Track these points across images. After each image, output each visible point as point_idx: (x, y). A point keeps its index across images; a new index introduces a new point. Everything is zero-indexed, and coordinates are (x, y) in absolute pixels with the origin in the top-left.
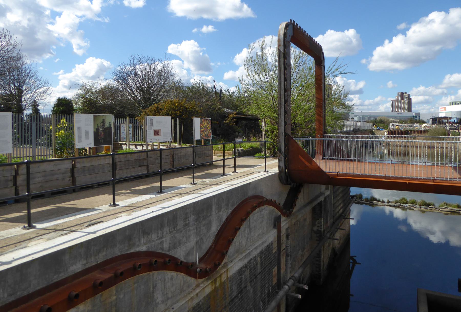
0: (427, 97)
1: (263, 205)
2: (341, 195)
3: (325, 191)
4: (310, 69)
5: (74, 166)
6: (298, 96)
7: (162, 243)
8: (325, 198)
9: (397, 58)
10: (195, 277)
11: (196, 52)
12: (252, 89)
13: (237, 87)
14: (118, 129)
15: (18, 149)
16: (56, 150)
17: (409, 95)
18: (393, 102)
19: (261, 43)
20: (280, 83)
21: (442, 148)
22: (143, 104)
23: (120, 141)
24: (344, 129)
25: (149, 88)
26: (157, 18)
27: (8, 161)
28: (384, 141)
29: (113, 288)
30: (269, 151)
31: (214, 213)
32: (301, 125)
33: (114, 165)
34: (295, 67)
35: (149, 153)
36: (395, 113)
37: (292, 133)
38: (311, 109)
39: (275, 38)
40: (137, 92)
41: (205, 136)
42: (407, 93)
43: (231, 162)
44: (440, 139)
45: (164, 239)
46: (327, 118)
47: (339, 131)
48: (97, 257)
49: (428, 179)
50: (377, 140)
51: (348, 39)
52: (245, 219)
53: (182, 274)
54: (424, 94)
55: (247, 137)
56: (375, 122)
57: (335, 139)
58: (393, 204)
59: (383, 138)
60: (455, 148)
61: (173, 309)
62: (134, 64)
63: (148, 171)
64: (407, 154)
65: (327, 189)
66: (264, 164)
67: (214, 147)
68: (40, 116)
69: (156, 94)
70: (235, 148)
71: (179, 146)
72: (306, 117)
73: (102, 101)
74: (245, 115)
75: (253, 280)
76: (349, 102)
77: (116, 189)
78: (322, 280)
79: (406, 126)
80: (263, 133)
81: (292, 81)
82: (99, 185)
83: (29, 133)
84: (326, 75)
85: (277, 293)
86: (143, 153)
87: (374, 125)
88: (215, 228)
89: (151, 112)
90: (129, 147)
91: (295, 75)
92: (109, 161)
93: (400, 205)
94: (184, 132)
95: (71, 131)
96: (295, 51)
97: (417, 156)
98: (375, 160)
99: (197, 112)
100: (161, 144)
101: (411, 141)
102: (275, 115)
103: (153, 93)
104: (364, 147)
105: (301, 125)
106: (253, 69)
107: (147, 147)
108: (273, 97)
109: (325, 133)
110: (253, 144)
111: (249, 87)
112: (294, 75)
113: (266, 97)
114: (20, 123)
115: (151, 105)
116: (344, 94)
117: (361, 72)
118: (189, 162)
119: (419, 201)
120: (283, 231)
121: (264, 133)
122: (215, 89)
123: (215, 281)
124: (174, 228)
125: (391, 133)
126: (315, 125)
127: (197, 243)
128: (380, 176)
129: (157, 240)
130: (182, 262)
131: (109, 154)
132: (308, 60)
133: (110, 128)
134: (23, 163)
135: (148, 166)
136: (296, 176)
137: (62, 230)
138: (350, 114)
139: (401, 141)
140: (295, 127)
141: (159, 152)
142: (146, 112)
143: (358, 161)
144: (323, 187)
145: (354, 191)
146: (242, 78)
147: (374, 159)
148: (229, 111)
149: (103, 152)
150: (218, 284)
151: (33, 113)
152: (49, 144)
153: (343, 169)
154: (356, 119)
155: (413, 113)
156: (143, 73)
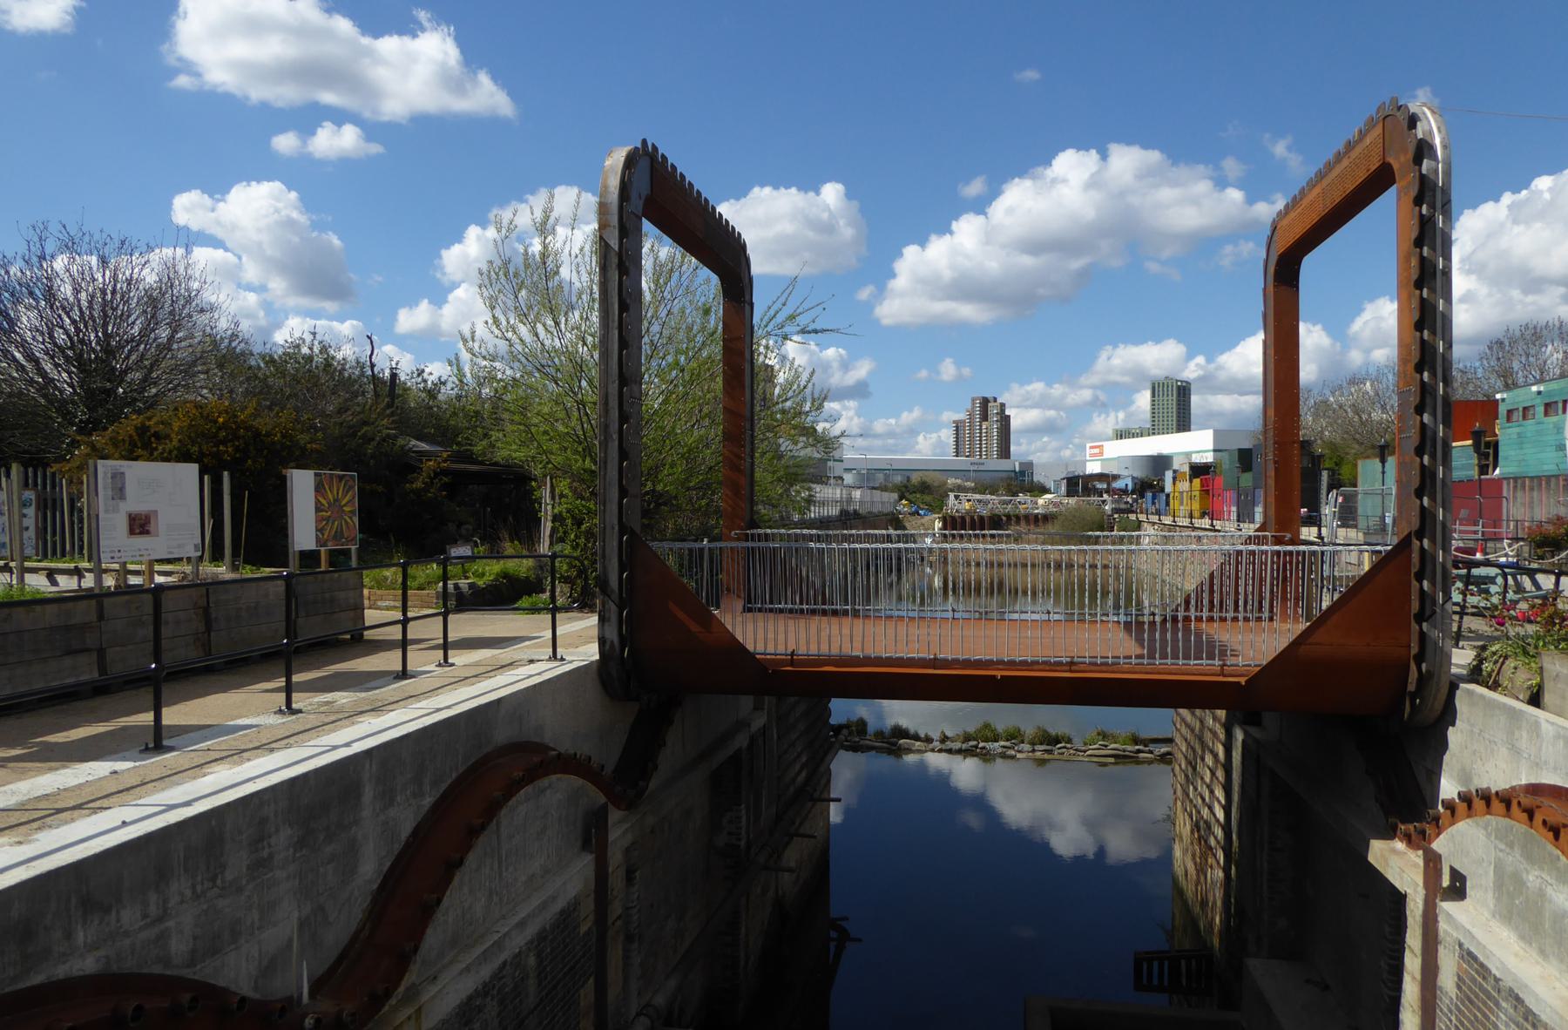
0: (1052, 413)
1: (547, 775)
4: (707, 312)
8: (752, 739)
9: (965, 288)
11: (290, 224)
12: (505, 371)
13: (455, 362)
17: (1003, 406)
18: (958, 427)
19: (538, 214)
20: (605, 355)
21: (1093, 566)
22: (81, 414)
24: (814, 513)
28: (930, 550)
31: (366, 813)
34: (659, 300)
35: (107, 601)
36: (963, 462)
37: (644, 527)
38: (707, 446)
39: (590, 200)
41: (335, 537)
42: (1000, 400)
46: (757, 475)
47: (796, 517)
51: (825, 216)
52: (483, 827)
57: (784, 544)
58: (957, 745)
59: (928, 540)
60: (1129, 568)
64: (999, 589)
66: (549, 634)
67: (368, 577)
70: (445, 578)
71: (230, 576)
72: (690, 472)
74: (482, 463)
76: (827, 425)
79: (994, 503)
81: (646, 349)
84: (758, 332)
86: (83, 604)
88: (370, 867)
89: (115, 445)
90: (21, 579)
91: (655, 328)
94: (252, 523)
96: (657, 249)
97: (1025, 593)
98: (908, 609)
99: (303, 449)
100: (157, 568)
104: (872, 569)
106: (510, 303)
107: (99, 580)
110: (511, 565)
111: (497, 365)
112: (653, 330)
113: (557, 403)
115: (114, 417)
116: (814, 400)
117: (858, 330)
118: (272, 631)
119: (1029, 731)
120: (615, 858)
121: (549, 524)
122: (373, 366)
124: (213, 879)
125: (951, 522)
126: (720, 499)
127: (302, 924)
130: (243, 1000)
132: (699, 280)
135: (101, 653)
136: (660, 671)
138: (830, 464)
139: (979, 548)
140: (657, 504)
141: (149, 597)
143: (856, 614)
144: (747, 702)
145: (842, 709)
146: (473, 333)
147: (904, 605)
148: (424, 446)
153: (808, 643)
154: (849, 478)
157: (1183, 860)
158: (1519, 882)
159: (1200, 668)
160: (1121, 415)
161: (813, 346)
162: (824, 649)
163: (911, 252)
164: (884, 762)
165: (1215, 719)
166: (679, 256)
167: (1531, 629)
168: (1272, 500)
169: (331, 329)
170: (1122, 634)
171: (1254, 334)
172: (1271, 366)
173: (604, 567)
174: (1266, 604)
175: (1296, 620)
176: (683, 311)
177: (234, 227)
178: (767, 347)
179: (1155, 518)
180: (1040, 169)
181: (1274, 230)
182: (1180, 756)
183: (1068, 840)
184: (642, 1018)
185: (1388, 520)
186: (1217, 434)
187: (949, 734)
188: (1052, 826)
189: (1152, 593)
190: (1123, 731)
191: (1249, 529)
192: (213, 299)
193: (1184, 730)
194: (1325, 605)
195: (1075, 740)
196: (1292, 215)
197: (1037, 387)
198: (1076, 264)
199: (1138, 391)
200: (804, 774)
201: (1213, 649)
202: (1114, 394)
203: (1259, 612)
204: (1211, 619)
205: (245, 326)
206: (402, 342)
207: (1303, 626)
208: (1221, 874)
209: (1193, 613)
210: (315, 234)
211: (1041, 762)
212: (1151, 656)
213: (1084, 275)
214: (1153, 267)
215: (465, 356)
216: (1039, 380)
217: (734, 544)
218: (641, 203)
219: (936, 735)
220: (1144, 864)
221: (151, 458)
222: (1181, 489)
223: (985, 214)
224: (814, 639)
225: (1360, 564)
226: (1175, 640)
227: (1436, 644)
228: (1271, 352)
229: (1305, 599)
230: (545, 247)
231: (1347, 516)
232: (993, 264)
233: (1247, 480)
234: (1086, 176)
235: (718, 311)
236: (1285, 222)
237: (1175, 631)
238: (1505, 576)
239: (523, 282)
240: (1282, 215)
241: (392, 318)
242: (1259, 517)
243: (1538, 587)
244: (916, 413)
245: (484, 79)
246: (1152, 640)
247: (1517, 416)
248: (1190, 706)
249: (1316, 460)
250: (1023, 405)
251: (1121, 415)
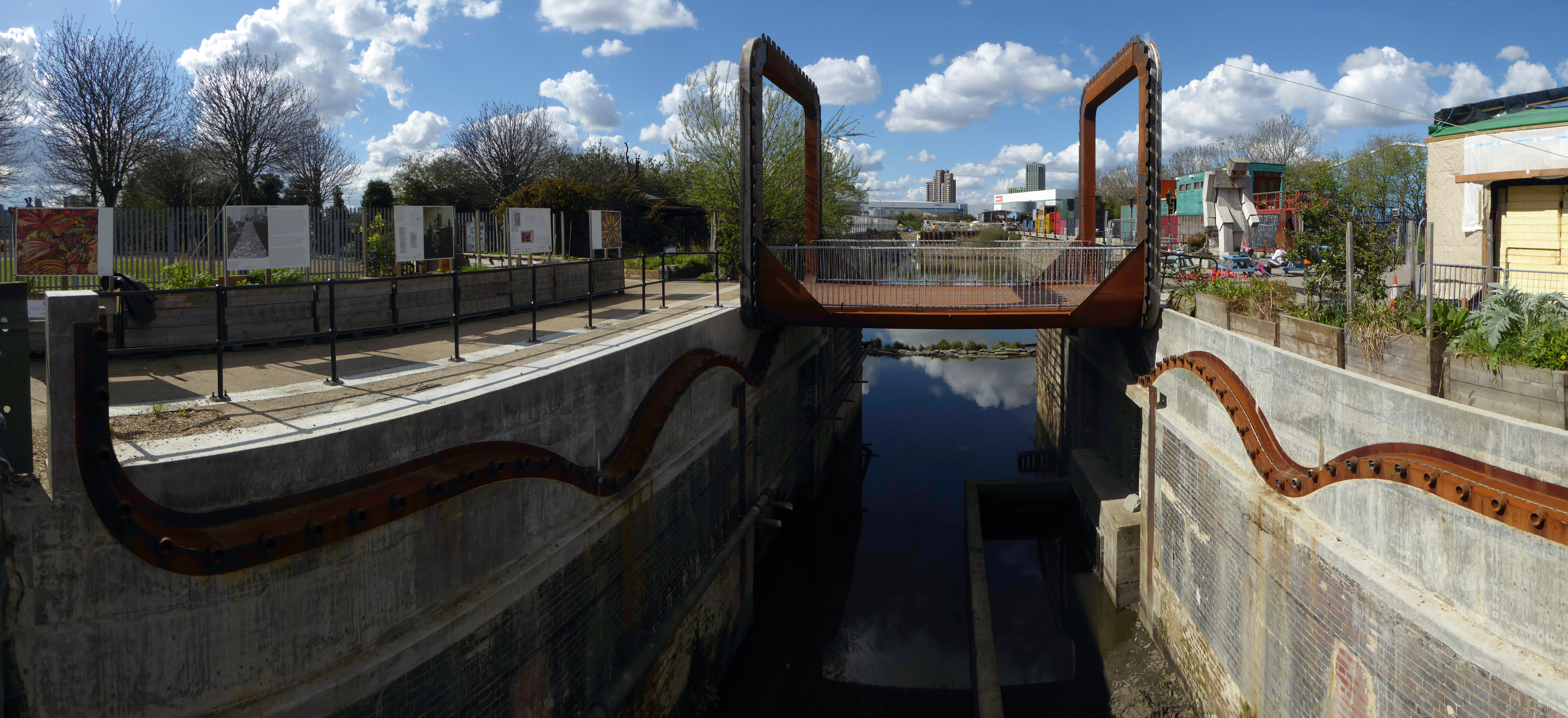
0: (977, 179)
1: (714, 366)
3: (820, 336)
4: (797, 125)
5: (394, 291)
6: (775, 172)
7: (537, 429)
8: (821, 350)
9: (933, 113)
10: (595, 493)
11: (590, 91)
12: (692, 158)
13: (667, 154)
14: (461, 230)
15: (317, 262)
16: (369, 264)
17: (952, 175)
18: (929, 186)
20: (743, 148)
21: (998, 258)
22: (502, 187)
23: (465, 251)
24: (853, 231)
25: (513, 158)
26: (524, 40)
27: (304, 280)
28: (914, 250)
29: (459, 498)
30: (724, 269)
31: (627, 380)
32: (781, 223)
33: (456, 292)
34: (771, 119)
35: (513, 272)
36: (931, 204)
37: (764, 238)
38: (797, 196)
39: (735, 67)
40: (492, 166)
43: (656, 289)
44: (995, 245)
45: (541, 423)
46: (824, 211)
47: (844, 233)
48: (432, 444)
51: (859, 73)
52: (683, 392)
53: (572, 486)
54: (971, 174)
55: (685, 245)
56: (901, 219)
58: (928, 352)
59: (913, 245)
60: (1015, 258)
61: (557, 546)
62: (486, 118)
63: (512, 304)
64: (949, 271)
66: (715, 293)
67: (626, 263)
68: (345, 211)
69: (524, 168)
70: (663, 264)
71: (564, 261)
72: (788, 210)
73: (436, 184)
74: (681, 205)
76: (860, 185)
77: (460, 332)
79: (947, 225)
80: (714, 238)
81: (765, 145)
82: (432, 325)
83: (331, 236)
84: (824, 135)
85: (740, 520)
86: (504, 273)
88: (629, 407)
89: (516, 201)
90: (480, 261)
91: (770, 134)
92: (449, 284)
94: (573, 237)
95: (390, 234)
96: (770, 92)
97: (963, 272)
98: (903, 281)
99: (596, 200)
100: (534, 257)
101: (955, 249)
102: (735, 205)
103: (519, 167)
104: (884, 260)
105: (781, 223)
107: (510, 262)
108: (731, 174)
109: (822, 237)
110: (695, 257)
111: (689, 155)
112: (768, 135)
113: (718, 174)
114: (318, 222)
115: (515, 188)
116: (853, 171)
117: (876, 134)
119: (965, 343)
120: (749, 411)
121: (715, 237)
122: (628, 158)
123: (630, 501)
124: (559, 405)
125: (926, 236)
126: (804, 223)
127: (598, 432)
129: (529, 424)
130: (572, 464)
131: (448, 272)
132: (793, 108)
133: (449, 229)
134: (324, 283)
135: (511, 295)
136: (774, 311)
137: (380, 392)
138: (862, 205)
139: (939, 249)
140: (771, 226)
141: (530, 271)
142: (507, 202)
143: (875, 284)
144: (818, 330)
145: (869, 334)
146: (676, 139)
147: (900, 279)
148: (652, 197)
149: (439, 270)
150: (635, 506)
151: (335, 205)
152: (359, 256)
153: (850, 299)
154: (871, 213)
155: (958, 205)
156: (502, 134)
157: (1041, 404)
158: (1187, 395)
159: (1049, 308)
160: (1012, 181)
161: (853, 143)
162: (859, 302)
163: (904, 93)
164: (891, 361)
165: (1056, 333)
166: (782, 95)
167: (1191, 282)
168: (1083, 224)
169: (608, 140)
170: (1012, 292)
171: (1075, 143)
172: (1083, 159)
173: (743, 259)
174: (1080, 275)
175: (1094, 283)
176: (784, 124)
177: (566, 94)
178: (828, 143)
179: (1028, 233)
180: (971, 52)
181: (1084, 92)
182: (1040, 352)
183: (985, 399)
184: (764, 496)
185: (1134, 235)
186: (1058, 192)
187: (924, 346)
188: (977, 392)
189: (1026, 271)
190: (1012, 342)
191: (1072, 239)
192: (555, 130)
193: (1042, 339)
194: (1106, 275)
195: (989, 347)
196: (1093, 86)
197: (969, 166)
198: (990, 102)
199: (1020, 169)
200: (848, 368)
201: (1056, 299)
202: (1008, 171)
203: (1077, 279)
204: (1054, 284)
205: (570, 142)
206: (643, 145)
207: (1097, 285)
208: (1059, 410)
209: (1046, 281)
210: (601, 95)
211: (972, 359)
212: (1026, 303)
213: (993, 109)
214: (1027, 106)
215: (673, 151)
216: (971, 162)
217: (811, 247)
218: (762, 68)
219: (917, 347)
220: (1023, 408)
221: (530, 207)
222: (1041, 219)
223: (943, 74)
224: (853, 297)
225: (1122, 255)
226: (1037, 295)
228: (1083, 152)
229: (1098, 273)
230: (712, 93)
231: (1116, 233)
232: (947, 101)
233: (1071, 214)
234: (995, 57)
235: (803, 124)
236: (1089, 89)
237: (1032, 290)
238: (1180, 259)
239: (702, 112)
240: (1088, 85)
241: (638, 134)
242: (1077, 233)
243: (1192, 264)
244: (907, 178)
245: (681, 7)
246: (1026, 295)
247: (1184, 188)
248: (1045, 327)
249: (1103, 205)
250: (962, 175)
251: (1012, 181)
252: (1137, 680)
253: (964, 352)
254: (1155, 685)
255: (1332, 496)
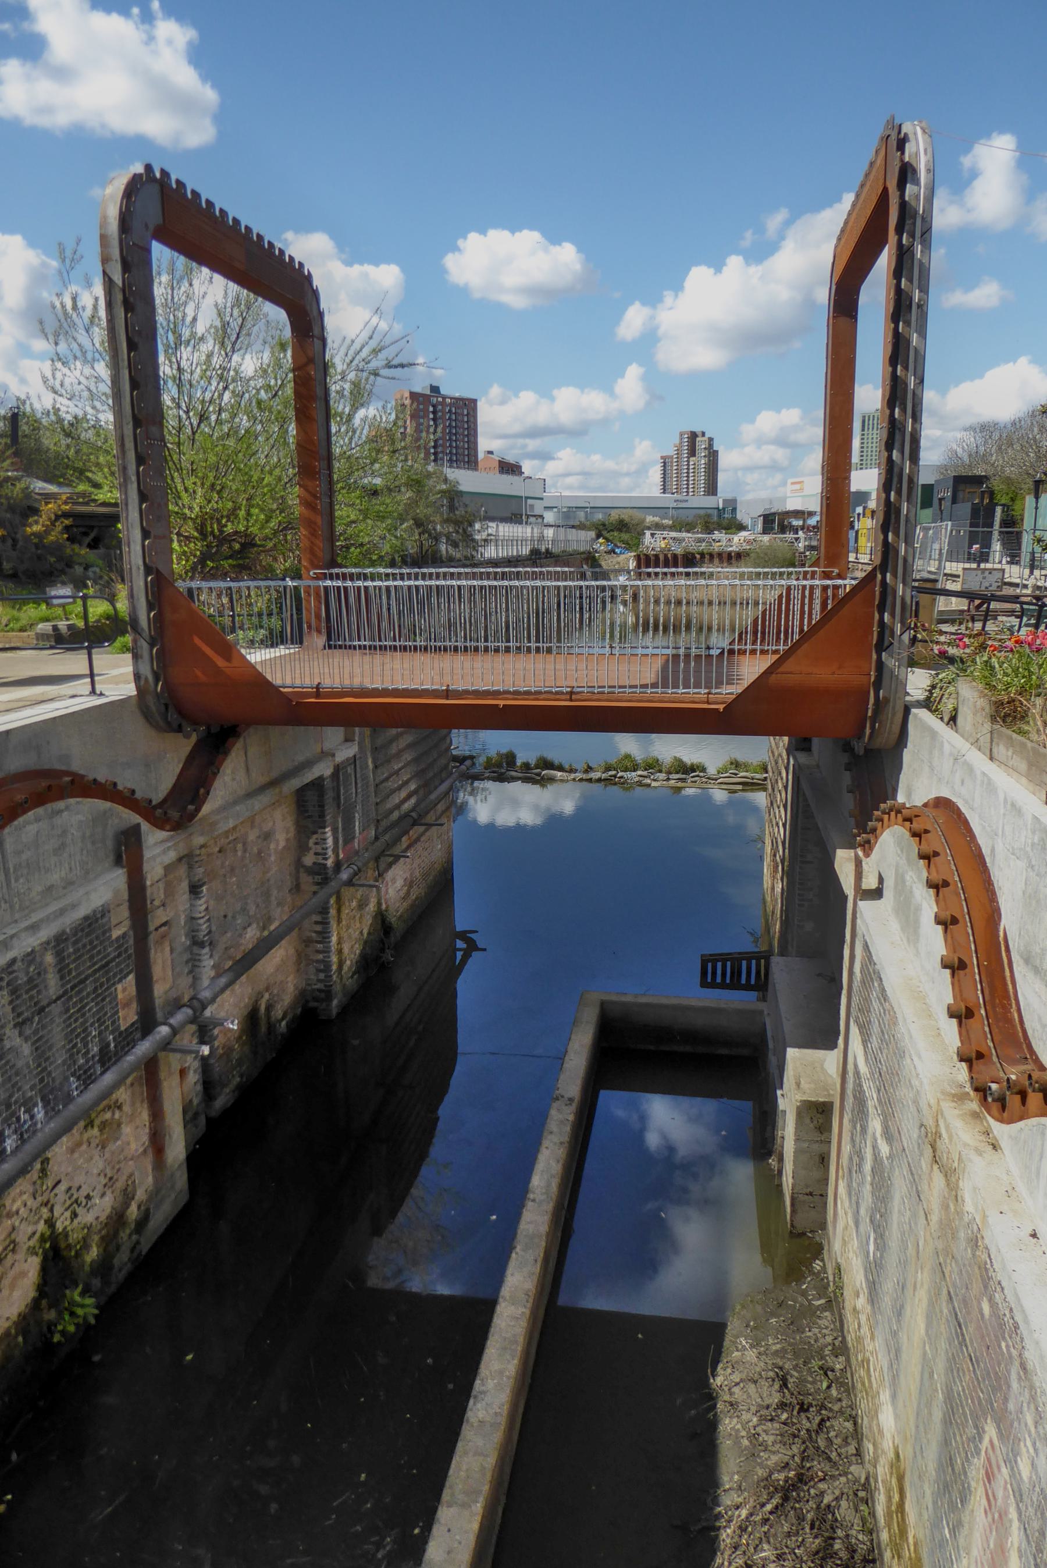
2: (408, 756)
8: (337, 769)
17: (711, 440)
28: (624, 588)
36: (669, 500)
42: (707, 435)
49: (557, 693)
50: (605, 583)
56: (601, 530)
65: (348, 739)
75: (29, 1020)
78: (335, 1002)
79: (689, 541)
87: (598, 536)
93: (615, 776)
109: (333, 564)
128: (413, 690)
139: (670, 585)
145: (462, 741)
154: (549, 517)
162: (347, 682)
200: (413, 801)
227: (892, 672)
236: (839, 249)
252: (778, 1346)
253: (662, 776)
254: (805, 1363)
255: (1039, 1143)
